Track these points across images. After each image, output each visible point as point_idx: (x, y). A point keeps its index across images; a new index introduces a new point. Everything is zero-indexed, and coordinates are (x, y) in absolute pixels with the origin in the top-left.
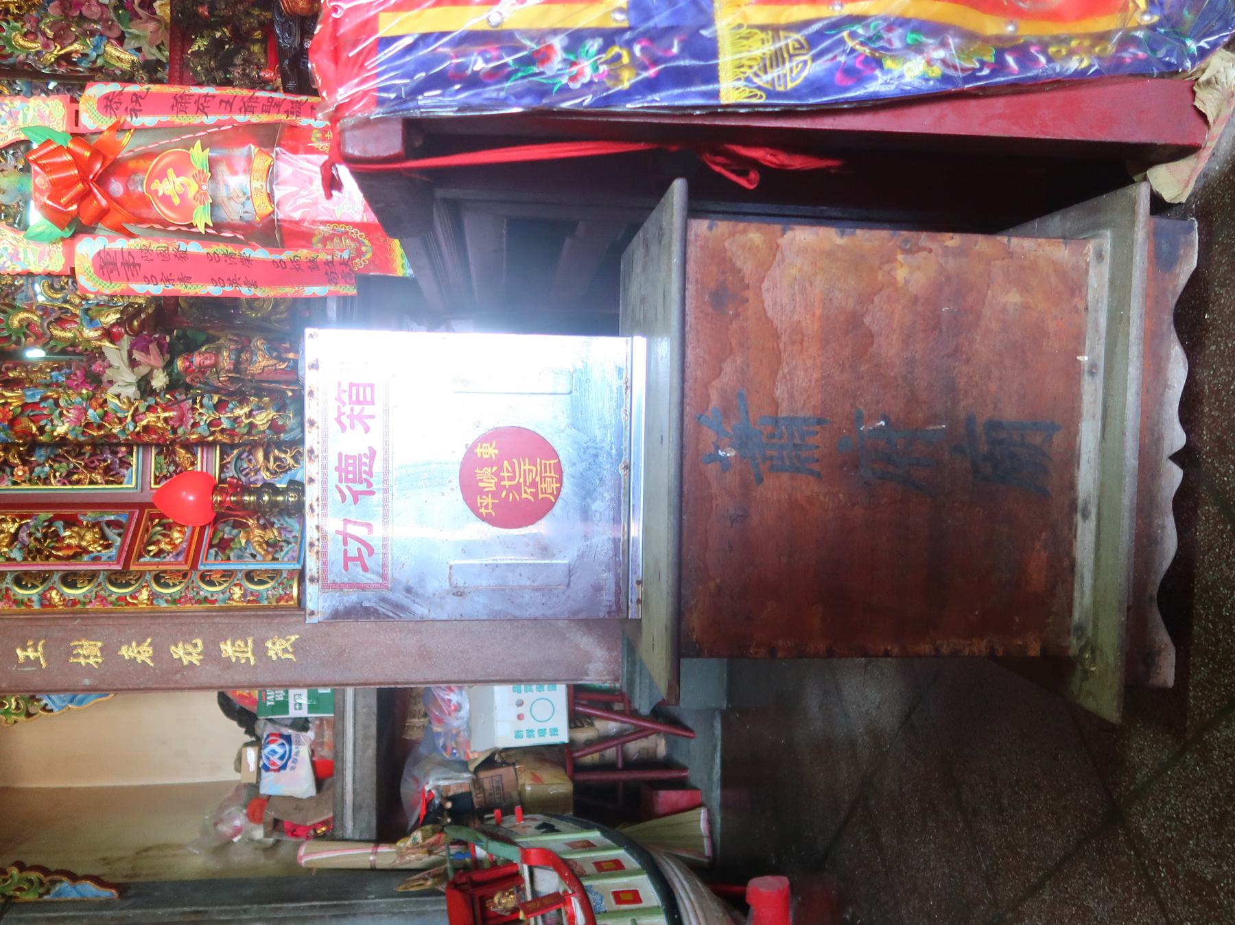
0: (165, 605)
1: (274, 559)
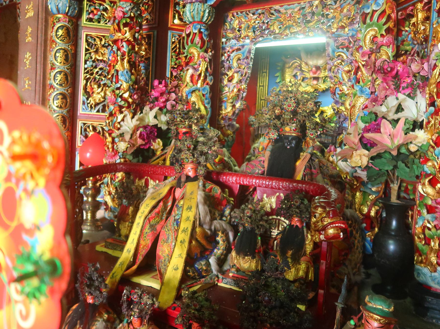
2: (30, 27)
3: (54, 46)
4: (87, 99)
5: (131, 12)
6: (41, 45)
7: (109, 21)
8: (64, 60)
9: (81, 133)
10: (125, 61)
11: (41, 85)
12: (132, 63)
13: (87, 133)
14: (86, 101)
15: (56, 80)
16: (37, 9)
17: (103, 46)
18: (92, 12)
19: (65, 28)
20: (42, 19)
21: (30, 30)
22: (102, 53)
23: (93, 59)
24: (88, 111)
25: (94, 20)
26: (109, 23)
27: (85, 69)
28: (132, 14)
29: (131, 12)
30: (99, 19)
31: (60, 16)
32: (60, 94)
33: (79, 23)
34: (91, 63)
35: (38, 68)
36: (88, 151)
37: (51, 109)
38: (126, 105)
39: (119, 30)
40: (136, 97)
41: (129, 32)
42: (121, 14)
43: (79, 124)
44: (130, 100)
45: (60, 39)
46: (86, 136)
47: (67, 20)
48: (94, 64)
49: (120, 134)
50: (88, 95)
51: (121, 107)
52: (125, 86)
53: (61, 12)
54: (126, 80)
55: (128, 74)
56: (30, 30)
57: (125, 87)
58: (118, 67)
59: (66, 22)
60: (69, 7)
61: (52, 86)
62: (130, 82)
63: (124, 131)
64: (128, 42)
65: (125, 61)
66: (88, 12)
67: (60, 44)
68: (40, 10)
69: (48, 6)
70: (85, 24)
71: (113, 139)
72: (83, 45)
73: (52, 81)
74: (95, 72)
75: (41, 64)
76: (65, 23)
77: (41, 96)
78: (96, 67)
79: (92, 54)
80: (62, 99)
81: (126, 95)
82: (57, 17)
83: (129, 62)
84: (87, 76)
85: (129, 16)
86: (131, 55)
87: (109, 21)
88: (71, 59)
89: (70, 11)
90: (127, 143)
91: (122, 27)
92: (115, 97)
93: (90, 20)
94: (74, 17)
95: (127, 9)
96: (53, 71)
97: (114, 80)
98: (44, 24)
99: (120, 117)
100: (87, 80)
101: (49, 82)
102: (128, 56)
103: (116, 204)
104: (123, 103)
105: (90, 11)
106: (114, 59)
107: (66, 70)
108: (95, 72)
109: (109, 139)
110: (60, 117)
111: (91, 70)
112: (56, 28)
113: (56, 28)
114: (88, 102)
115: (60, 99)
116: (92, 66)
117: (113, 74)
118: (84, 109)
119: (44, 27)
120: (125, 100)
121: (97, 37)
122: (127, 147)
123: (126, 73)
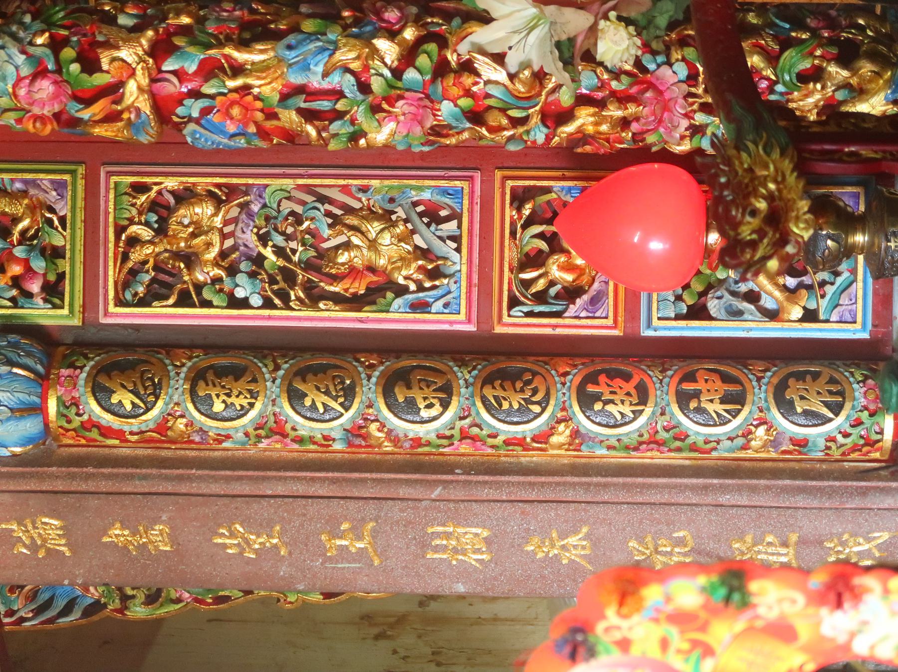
0: (604, 452)
1: (810, 316)
2: (105, 533)
3: (181, 424)
4: (401, 291)
5: (31, 44)
6: (180, 478)
7: (52, 210)
8: (242, 381)
9: (558, 315)
10: (241, 56)
11: (356, 475)
12: (247, 35)
13: (553, 291)
14: (410, 297)
15: (324, 422)
16: (33, 500)
17: (161, 231)
18: (16, 282)
19: (103, 380)
20: (73, 477)
21: (117, 534)
22: (194, 235)
23: (223, 274)
24: (453, 287)
25: (52, 277)
26: (57, 207)
27: (268, 304)
28: (40, 41)
29: (31, 44)
30: (43, 252)
31: (52, 405)
32: (388, 393)
33: (69, 339)
34: (241, 278)
35: (280, 489)
36: (641, 250)
37: (456, 432)
38: (432, 47)
39: (114, 90)
40: (392, 15)
41: (118, 48)
42: (46, 87)
43: (514, 323)
44: (409, 34)
45: (152, 399)
46: (571, 293)
47: (65, 372)
48: (244, 266)
49: (568, 63)
50: (381, 289)
51: (441, 69)
52: (347, 55)
53: (36, 400)
54: (323, 50)
55: (300, 43)
56: (117, 534)
57: (352, 55)
58: (267, 89)
59: (74, 380)
60: (11, 363)
61: (356, 432)
62: (332, 36)
63: (549, 46)
64: (160, 50)
65: (241, 56)
66: (21, 301)
67: (174, 404)
68: (33, 485)
69: (15, 455)
70: (71, 311)
71: (583, 100)
72: (165, 314)
73: (335, 429)
74: (281, 263)
75: (264, 479)
76: (81, 382)
77: (403, 476)
78: (259, 260)
79: (201, 277)
80: (409, 387)
81: (388, 49)
82: (60, 415)
83: (244, 44)
84: (298, 299)
85: (48, 51)
86: (216, 37)
87: (52, 210)
88: (226, 360)
89: (29, 362)
90: (602, 24)
91: (100, 80)
92: (401, 97)
93: (53, 291)
94: (50, 356)
95: (20, 59)
96: (288, 427)
97: (324, 105)
98: (91, 470)
99: (488, 70)
100: (314, 297)
101: (338, 446)
102: (221, 45)
103: (878, 74)
104: (423, 61)
105: (14, 292)
106: (236, 111)
107: (281, 372)
108: (281, 263)
109: (584, 118)
110: (489, 392)
111: (272, 281)
112: (107, 419)
113: (107, 419)
114: (413, 287)
115: (410, 394)
116: (252, 275)
117: (300, 111)
118: (446, 305)
119: (106, 471)
120: (409, 57)
121: (125, 257)
122: (620, 18)
123: (293, 53)
